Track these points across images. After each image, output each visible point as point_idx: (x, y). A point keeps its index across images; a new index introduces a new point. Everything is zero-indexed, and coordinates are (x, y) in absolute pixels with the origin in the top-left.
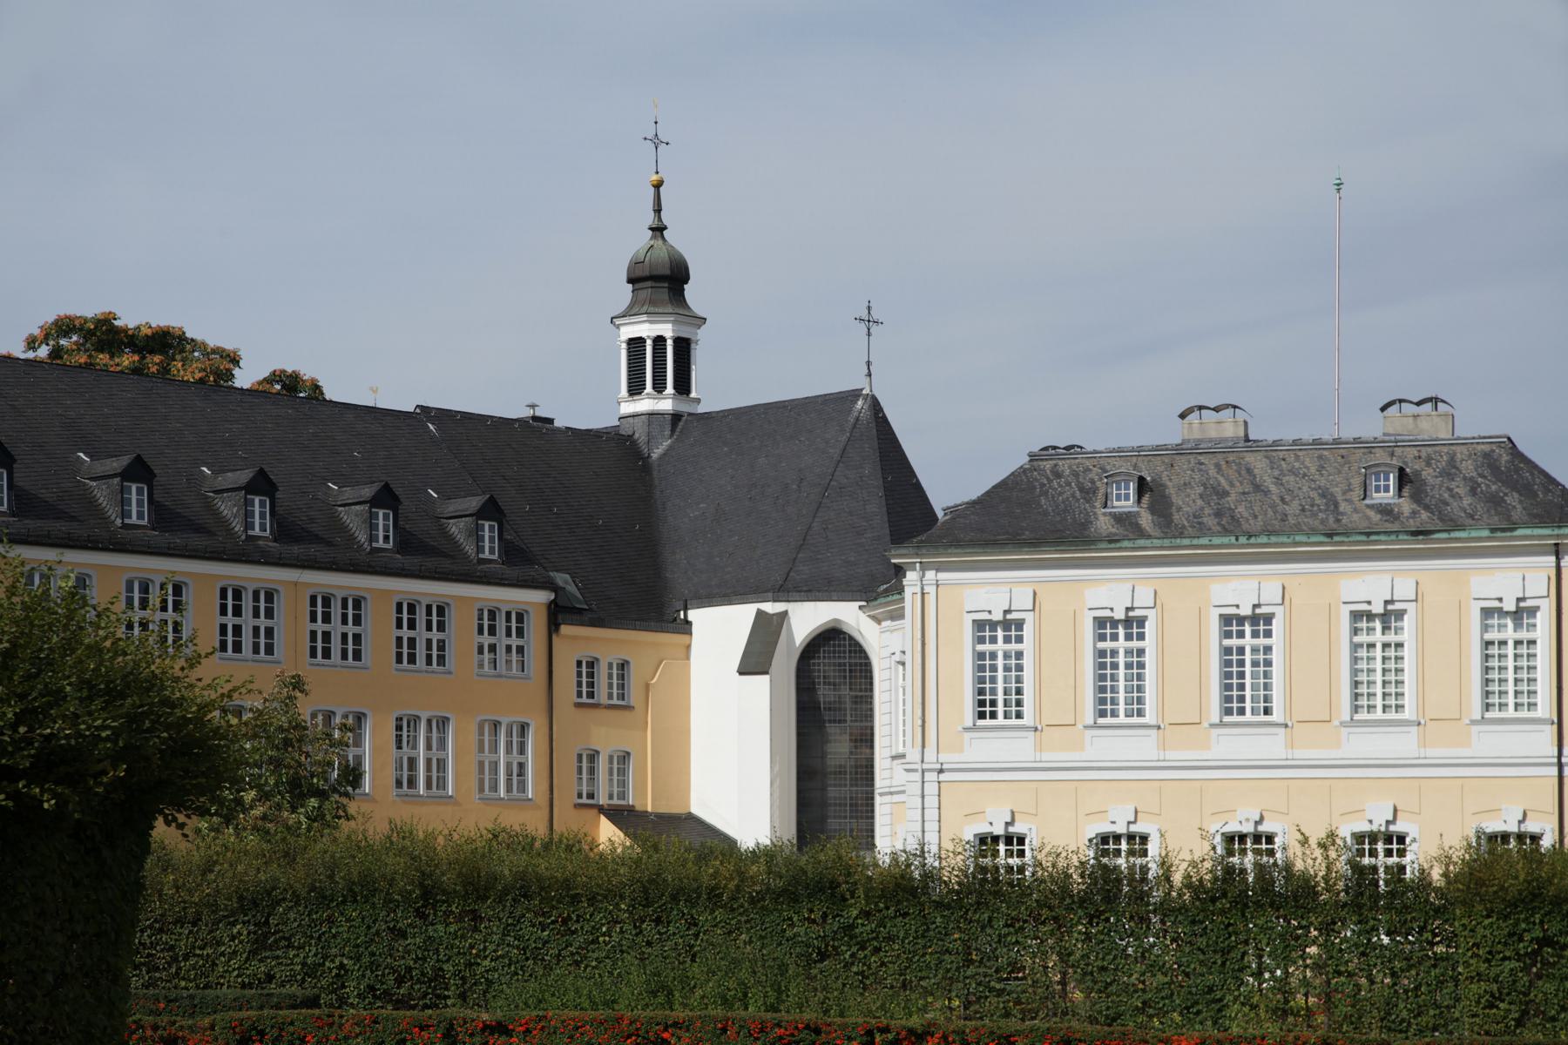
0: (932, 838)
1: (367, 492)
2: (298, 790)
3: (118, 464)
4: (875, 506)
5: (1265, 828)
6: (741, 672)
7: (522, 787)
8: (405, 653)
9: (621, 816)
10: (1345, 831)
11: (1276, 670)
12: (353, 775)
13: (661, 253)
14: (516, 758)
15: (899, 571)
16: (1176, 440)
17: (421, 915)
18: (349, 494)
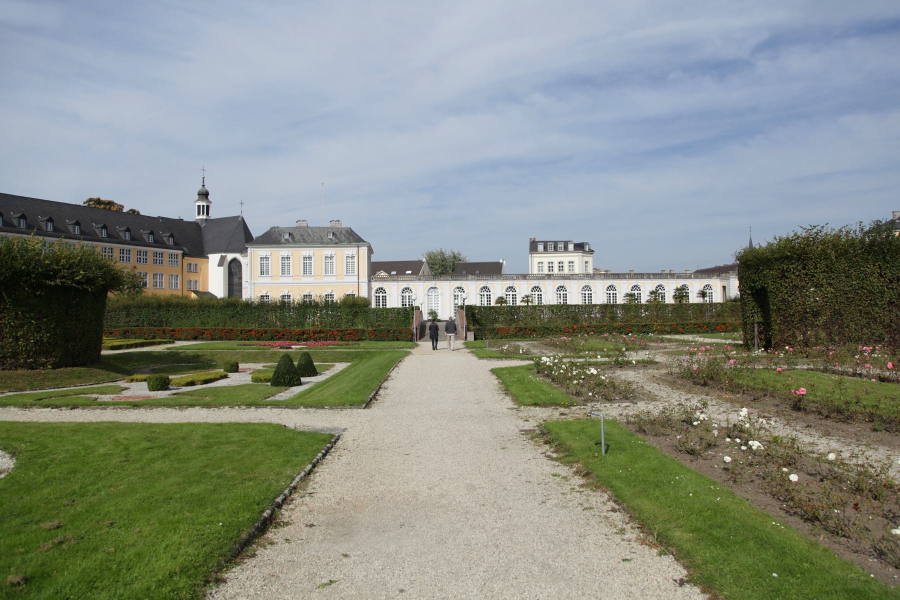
0: (252, 296)
1: (148, 232)
2: (134, 287)
3: (100, 226)
4: (242, 236)
5: (268, 294)
6: (219, 266)
7: (177, 287)
8: (155, 262)
9: (196, 292)
10: (324, 295)
11: (312, 266)
12: (145, 284)
13: (204, 190)
14: (161, 280)
15: (247, 248)
16: (295, 226)
17: (158, 310)
18: (145, 232)
